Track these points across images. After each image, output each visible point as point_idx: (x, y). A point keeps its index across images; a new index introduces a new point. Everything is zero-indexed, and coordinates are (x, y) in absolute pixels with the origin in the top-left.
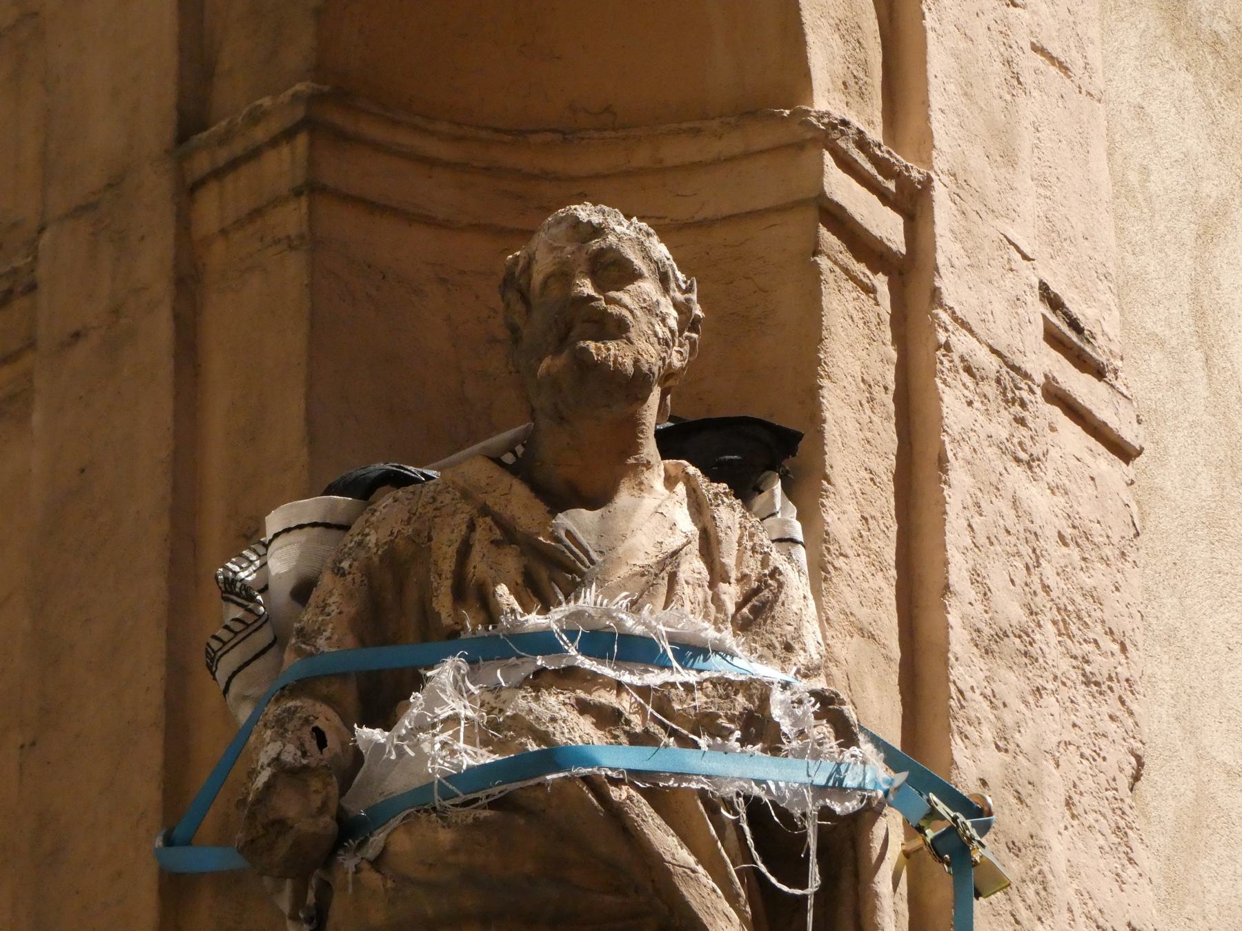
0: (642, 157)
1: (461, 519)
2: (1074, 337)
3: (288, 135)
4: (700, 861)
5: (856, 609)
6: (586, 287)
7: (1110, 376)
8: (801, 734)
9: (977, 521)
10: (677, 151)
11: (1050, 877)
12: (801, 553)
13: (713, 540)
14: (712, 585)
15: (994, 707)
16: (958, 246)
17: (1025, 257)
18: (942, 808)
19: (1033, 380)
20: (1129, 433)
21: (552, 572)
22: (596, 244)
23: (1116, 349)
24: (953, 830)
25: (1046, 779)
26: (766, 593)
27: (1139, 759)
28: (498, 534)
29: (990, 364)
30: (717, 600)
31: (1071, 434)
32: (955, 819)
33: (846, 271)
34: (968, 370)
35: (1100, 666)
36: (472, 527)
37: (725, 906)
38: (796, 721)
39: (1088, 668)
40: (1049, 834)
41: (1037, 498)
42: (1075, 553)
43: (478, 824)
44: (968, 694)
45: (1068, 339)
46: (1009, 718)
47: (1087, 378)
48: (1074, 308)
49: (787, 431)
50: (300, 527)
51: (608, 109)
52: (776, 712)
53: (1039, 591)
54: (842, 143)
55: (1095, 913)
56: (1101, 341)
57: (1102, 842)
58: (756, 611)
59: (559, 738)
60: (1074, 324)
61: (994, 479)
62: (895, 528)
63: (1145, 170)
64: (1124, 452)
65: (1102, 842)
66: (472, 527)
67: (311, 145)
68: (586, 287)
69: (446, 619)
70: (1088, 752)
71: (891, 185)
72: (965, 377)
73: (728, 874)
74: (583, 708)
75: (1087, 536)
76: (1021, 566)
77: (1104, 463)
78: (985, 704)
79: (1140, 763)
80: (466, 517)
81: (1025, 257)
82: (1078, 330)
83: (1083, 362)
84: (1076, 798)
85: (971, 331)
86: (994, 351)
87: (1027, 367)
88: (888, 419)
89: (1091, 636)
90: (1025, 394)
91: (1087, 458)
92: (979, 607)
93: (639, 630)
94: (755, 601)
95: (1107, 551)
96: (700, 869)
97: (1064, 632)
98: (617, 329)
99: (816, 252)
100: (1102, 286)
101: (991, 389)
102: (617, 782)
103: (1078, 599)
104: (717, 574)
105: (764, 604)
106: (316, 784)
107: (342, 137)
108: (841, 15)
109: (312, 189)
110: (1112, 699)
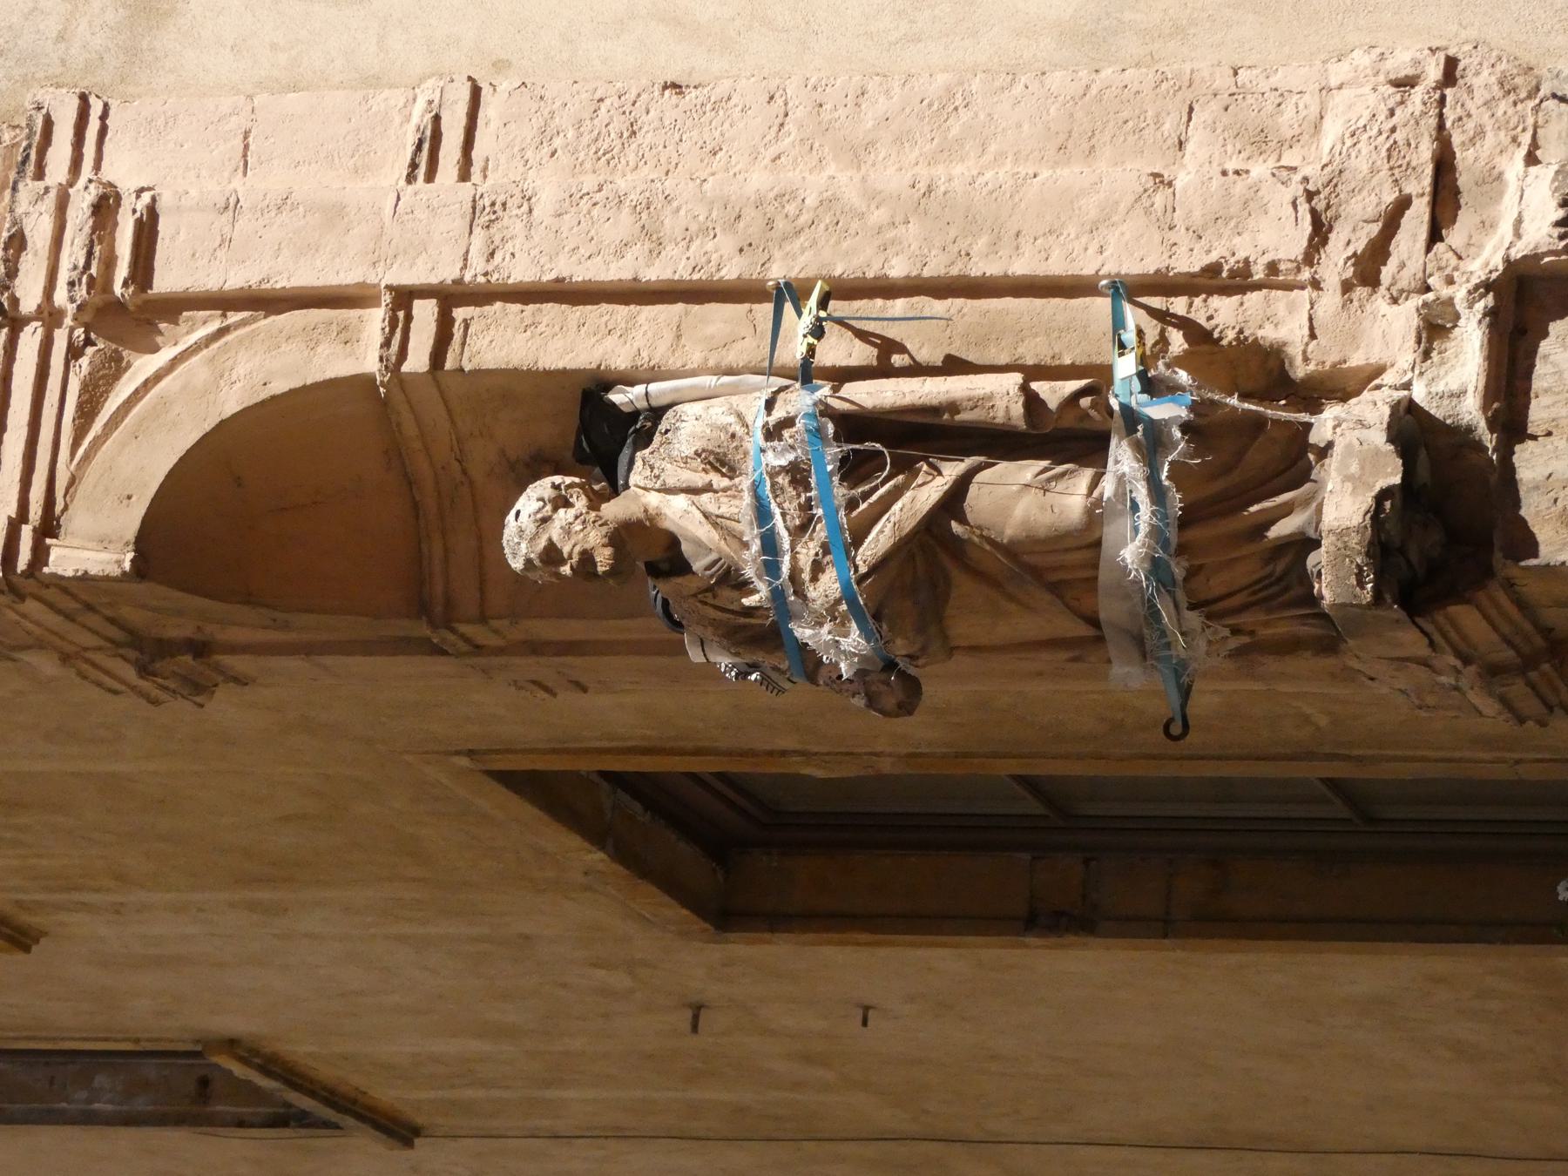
0: (417, 445)
2: (426, 146)
3: (453, 631)
6: (566, 570)
8: (792, 447)
10: (410, 429)
11: (775, 191)
13: (558, 286)
14: (716, 492)
17: (398, 198)
21: (732, 579)
22: (537, 562)
26: (711, 458)
27: (665, 87)
29: (479, 235)
30: (725, 490)
33: (463, 344)
34: (492, 254)
38: (784, 450)
45: (426, 155)
48: (410, 150)
51: (386, 452)
52: (783, 462)
54: (393, 359)
58: (723, 464)
59: (838, 595)
60: (419, 147)
62: (604, 306)
67: (460, 621)
68: (566, 570)
71: (401, 314)
73: (889, 492)
74: (814, 579)
81: (398, 198)
85: (467, 252)
88: (540, 310)
93: (758, 542)
98: (587, 557)
99: (462, 370)
102: (856, 568)
104: (708, 488)
105: (718, 460)
106: (874, 688)
107: (449, 603)
108: (303, 346)
109: (483, 619)
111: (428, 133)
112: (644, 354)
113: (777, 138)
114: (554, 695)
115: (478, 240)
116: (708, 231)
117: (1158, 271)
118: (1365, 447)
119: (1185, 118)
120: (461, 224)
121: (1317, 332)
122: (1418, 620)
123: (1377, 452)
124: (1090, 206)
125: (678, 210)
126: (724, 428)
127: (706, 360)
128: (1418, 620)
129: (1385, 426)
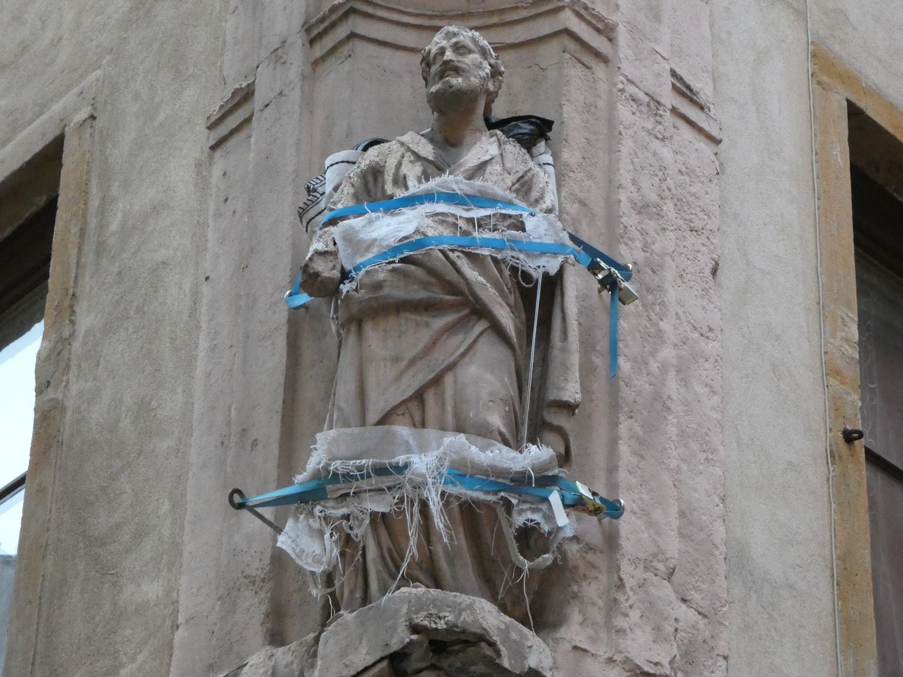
1: (398, 155)
4: (488, 281)
5: (578, 193)
7: (706, 110)
9: (636, 160)
12: (551, 169)
15: (642, 234)
16: (630, 52)
18: (603, 264)
19: (665, 106)
20: (715, 133)
23: (711, 100)
24: (610, 275)
25: (667, 265)
28: (412, 158)
31: (686, 133)
32: (609, 270)
35: (697, 224)
36: (403, 157)
37: (500, 300)
39: (692, 225)
40: (667, 286)
41: (666, 152)
42: (688, 179)
43: (394, 270)
44: (629, 228)
45: (685, 91)
46: (649, 239)
47: (698, 111)
49: (548, 121)
50: (337, 163)
53: (666, 190)
55: (692, 321)
56: (702, 95)
57: (696, 293)
60: (688, 87)
61: (645, 144)
63: (729, 33)
64: (716, 141)
65: (696, 293)
66: (403, 157)
69: (389, 192)
70: (691, 257)
72: (632, 103)
75: (693, 171)
76: (657, 179)
77: (703, 146)
78: (638, 233)
79: (717, 264)
80: (401, 153)
81: (663, 57)
82: (691, 90)
83: (693, 102)
84: (685, 275)
86: (647, 94)
87: (663, 101)
89: (694, 211)
90: (661, 112)
91: (693, 140)
92: (635, 194)
94: (522, 181)
95: (703, 179)
96: (488, 285)
97: (678, 209)
100: (705, 75)
101: (644, 109)
103: (688, 197)
110: (704, 236)
111: (695, 98)
112: (571, 174)
113: (689, 322)
114: (210, 128)
115: (641, 95)
116: (646, 248)
117: (621, 545)
118: (527, 650)
119: (700, 609)
120: (651, 89)
121: (578, 653)
122: (385, 664)
123: (524, 657)
124: (657, 515)
125: (658, 234)
126: (542, 197)
127: (567, 214)
128: (385, 664)
129: (540, 670)
